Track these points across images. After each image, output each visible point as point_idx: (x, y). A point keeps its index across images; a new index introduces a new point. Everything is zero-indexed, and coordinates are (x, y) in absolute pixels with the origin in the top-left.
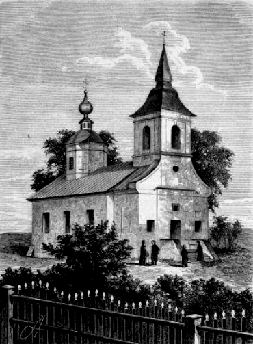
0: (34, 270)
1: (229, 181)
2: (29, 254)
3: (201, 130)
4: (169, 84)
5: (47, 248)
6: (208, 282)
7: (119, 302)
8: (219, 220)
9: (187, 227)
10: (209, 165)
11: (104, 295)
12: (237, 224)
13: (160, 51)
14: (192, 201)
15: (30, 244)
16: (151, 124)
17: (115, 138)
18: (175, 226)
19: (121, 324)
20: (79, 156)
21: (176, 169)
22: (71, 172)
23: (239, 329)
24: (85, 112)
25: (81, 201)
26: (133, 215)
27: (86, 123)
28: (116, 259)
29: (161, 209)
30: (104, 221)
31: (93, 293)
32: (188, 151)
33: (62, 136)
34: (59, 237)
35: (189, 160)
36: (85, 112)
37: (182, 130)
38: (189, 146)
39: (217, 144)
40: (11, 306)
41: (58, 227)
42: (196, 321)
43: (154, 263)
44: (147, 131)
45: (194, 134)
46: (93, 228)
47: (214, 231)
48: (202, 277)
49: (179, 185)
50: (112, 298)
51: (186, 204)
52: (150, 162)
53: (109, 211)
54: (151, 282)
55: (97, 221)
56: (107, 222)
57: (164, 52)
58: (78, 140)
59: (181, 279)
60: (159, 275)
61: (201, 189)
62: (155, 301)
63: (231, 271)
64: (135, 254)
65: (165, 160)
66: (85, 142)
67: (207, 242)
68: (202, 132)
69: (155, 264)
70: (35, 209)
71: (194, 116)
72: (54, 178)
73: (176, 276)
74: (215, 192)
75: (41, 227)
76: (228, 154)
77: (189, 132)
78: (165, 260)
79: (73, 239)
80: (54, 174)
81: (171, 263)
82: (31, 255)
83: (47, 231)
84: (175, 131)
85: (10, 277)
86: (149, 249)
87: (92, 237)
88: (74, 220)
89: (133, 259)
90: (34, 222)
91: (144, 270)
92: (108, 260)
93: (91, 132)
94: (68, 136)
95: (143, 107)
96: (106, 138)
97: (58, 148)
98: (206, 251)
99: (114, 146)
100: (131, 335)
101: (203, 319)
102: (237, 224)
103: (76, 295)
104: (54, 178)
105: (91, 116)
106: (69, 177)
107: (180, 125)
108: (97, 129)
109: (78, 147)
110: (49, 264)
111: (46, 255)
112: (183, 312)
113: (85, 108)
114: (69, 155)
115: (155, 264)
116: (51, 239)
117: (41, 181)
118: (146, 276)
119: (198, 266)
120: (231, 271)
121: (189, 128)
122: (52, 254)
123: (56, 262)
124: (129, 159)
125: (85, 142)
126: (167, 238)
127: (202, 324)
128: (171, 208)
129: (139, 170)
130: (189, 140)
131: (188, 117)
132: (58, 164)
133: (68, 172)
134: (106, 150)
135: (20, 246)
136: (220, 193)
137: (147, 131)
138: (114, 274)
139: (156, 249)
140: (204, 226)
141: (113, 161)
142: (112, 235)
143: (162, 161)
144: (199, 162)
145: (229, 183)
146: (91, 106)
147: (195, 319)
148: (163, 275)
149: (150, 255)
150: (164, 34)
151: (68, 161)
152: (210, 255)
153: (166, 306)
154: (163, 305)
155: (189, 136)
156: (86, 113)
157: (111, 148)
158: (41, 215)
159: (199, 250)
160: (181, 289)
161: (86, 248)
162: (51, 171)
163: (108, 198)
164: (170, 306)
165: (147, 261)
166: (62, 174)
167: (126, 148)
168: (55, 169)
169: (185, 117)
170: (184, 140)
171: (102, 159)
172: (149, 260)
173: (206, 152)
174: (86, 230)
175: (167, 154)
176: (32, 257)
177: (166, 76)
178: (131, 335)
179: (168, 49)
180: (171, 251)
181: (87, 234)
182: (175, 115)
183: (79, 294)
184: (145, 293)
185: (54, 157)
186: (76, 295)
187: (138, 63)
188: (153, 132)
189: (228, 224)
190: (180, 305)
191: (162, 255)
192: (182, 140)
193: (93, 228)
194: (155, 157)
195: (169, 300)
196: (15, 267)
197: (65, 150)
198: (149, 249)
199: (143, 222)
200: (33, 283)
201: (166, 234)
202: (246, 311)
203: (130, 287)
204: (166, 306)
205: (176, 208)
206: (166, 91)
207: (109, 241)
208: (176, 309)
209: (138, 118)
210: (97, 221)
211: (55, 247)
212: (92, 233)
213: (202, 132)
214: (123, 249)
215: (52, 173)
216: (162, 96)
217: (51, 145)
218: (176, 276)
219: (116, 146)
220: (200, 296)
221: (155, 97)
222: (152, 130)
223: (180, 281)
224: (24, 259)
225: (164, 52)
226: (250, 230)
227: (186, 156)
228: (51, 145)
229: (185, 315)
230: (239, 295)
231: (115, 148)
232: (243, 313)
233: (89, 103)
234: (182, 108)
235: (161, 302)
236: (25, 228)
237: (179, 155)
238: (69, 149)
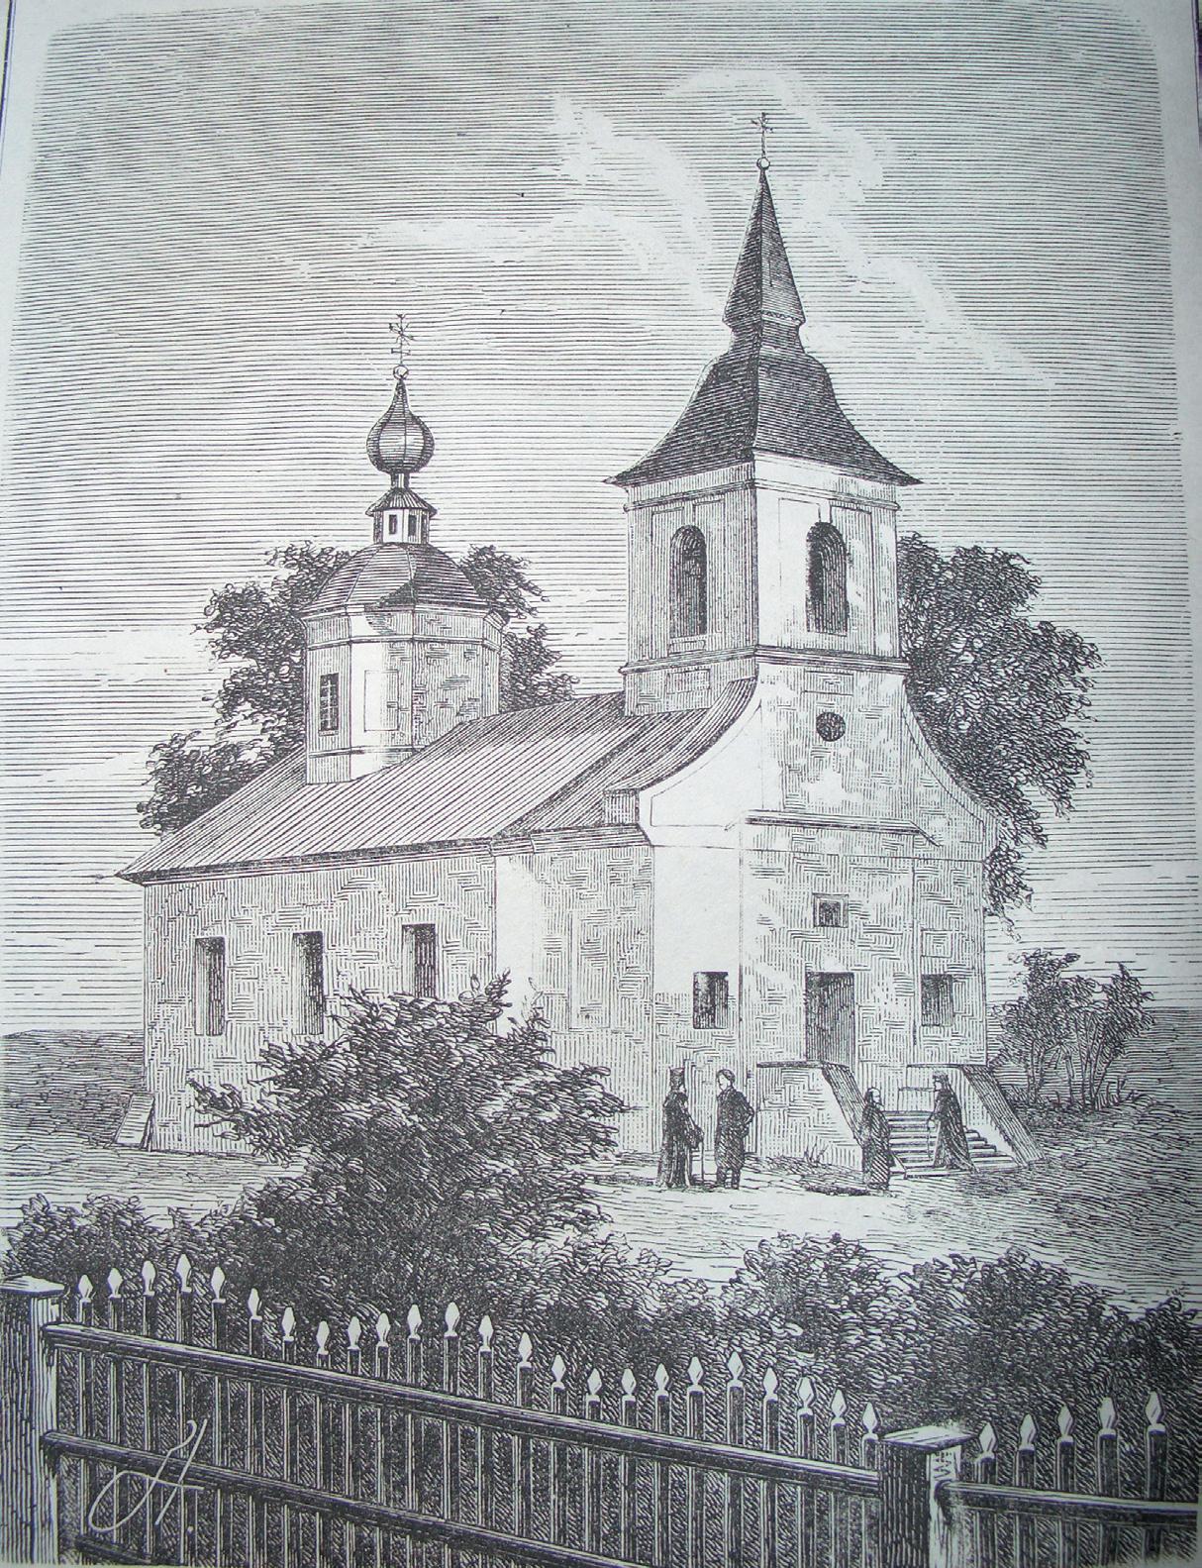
0: (156, 1213)
1: (1080, 780)
2: (131, 1133)
3: (946, 543)
4: (793, 335)
5: (218, 1103)
6: (989, 1269)
7: (559, 1367)
8: (1040, 967)
9: (885, 1002)
10: (985, 709)
11: (486, 1328)
12: (1125, 984)
13: (748, 195)
14: (906, 880)
15: (139, 1090)
16: (712, 521)
17: (541, 583)
18: (827, 990)
19: (428, 1446)
20: (364, 669)
21: (830, 727)
22: (327, 743)
23: (1047, 1482)
24: (401, 457)
25: (374, 879)
26: (621, 953)
27: (402, 516)
28: (544, 1159)
29: (764, 921)
30: (484, 983)
31: (433, 1324)
32: (886, 644)
33: (284, 573)
34: (271, 1055)
35: (893, 683)
36: (401, 457)
37: (857, 547)
38: (889, 619)
39: (1018, 612)
40: (48, 1381)
41: (270, 1002)
42: (932, 1462)
43: (728, 1178)
44: (693, 546)
45: (915, 557)
46: (430, 1011)
47: (1019, 1019)
48: (961, 1248)
49: (846, 804)
50: (525, 1347)
51: (878, 897)
52: (704, 694)
53: (517, 933)
54: (711, 1274)
55: (454, 984)
56: (499, 987)
57: (765, 193)
58: (359, 594)
59: (860, 1251)
60: (750, 1236)
61: (958, 824)
62: (735, 1364)
63: (1101, 1213)
64: (640, 1132)
65: (776, 685)
66: (403, 599)
67: (981, 1074)
68: (946, 553)
69: (735, 1184)
70: (163, 923)
71: (908, 480)
72: (249, 773)
73: (836, 1239)
74: (1016, 839)
75: (187, 1005)
76: (1075, 652)
77: (890, 555)
78: (780, 1164)
79: (338, 1064)
80: (250, 756)
81: (810, 1173)
82: (137, 1138)
83: (216, 1025)
84: (824, 541)
85: (52, 1246)
86: (704, 1111)
87: (430, 1053)
88: (343, 970)
89: (625, 1160)
90: (160, 986)
91: (679, 1209)
92: (508, 1165)
93: (426, 551)
94: (316, 573)
95: (670, 443)
96: (492, 581)
97: (267, 635)
98: (978, 1121)
99: (532, 621)
100: (615, 1529)
101: (969, 1445)
102: (1125, 984)
103: (354, 1329)
104: (249, 773)
105: (422, 483)
106: (319, 770)
107: (842, 520)
108: (454, 539)
109: (360, 626)
110: (228, 1178)
111: (205, 1140)
112: (869, 1419)
113: (394, 443)
114: (320, 663)
115: (735, 1184)
116: (239, 1066)
117: (189, 789)
118: (687, 1241)
119: (944, 1192)
120: (1101, 1213)
121: (887, 539)
122: (241, 1129)
123: (274, 1172)
124: (610, 682)
125: (403, 599)
126: (787, 1057)
127: (966, 1473)
128: (808, 914)
129: (652, 737)
130: (888, 593)
131: (880, 487)
132: (264, 705)
133: (317, 741)
134: (495, 640)
135: (81, 1091)
136: (1041, 840)
137: (693, 546)
138: (536, 1233)
139: (736, 1109)
140: (966, 996)
141: (530, 687)
142: (528, 1046)
143: (762, 692)
144: (940, 697)
145: (1079, 794)
146: (425, 431)
147: (930, 1450)
148: (769, 1235)
149: (708, 1139)
150: (763, 123)
151: (314, 692)
152: (995, 1138)
153: (786, 1388)
154: (770, 1381)
155: (887, 574)
156: (397, 467)
157: (519, 628)
158: (188, 946)
159: (948, 1107)
160: (859, 1303)
161: (399, 1107)
162: (232, 739)
163: (509, 870)
164: (805, 1390)
165: (696, 1171)
166: (287, 746)
167: (595, 617)
168: (250, 732)
169: (867, 487)
170: (871, 588)
171: (482, 681)
172: (705, 1164)
173: (969, 646)
174: (399, 1023)
175: (781, 655)
176: (141, 1147)
177: (775, 302)
178: (615, 1529)
179: (778, 185)
180: (812, 1120)
181: (403, 1039)
182: (824, 476)
183: (368, 1321)
184: (660, 1339)
185: (250, 673)
186: (354, 1329)
187: (639, 239)
188: (721, 560)
189: (1083, 985)
190: (854, 1383)
191: (768, 1138)
192: (856, 593)
193: (430, 1011)
194: (731, 671)
195: (802, 1359)
196: (70, 1195)
197: (301, 643)
198: (704, 1111)
199: (677, 981)
200: (148, 1272)
201: (789, 1038)
202: (1163, 1400)
203: (615, 1290)
204: (786, 1388)
205: (829, 914)
206: (774, 367)
207: (511, 1074)
208: (838, 1403)
209: (649, 491)
210: (454, 984)
211: (251, 1099)
212: (427, 1034)
213: (946, 553)
214: (579, 1108)
215: (236, 750)
216: (757, 399)
217: (239, 618)
218: (836, 1239)
219: (545, 618)
220: (955, 1337)
221: (728, 397)
222: (714, 551)
223: (854, 1264)
224: (102, 1157)
225: (765, 193)
226: (1181, 1013)
227: (881, 664)
228: (239, 618)
229: (881, 1431)
230: (1136, 1325)
231: (540, 633)
232: (1153, 1407)
233: (415, 420)
234: (839, 442)
235: (762, 1368)
236: (115, 1013)
237: (850, 662)
238: (318, 635)
